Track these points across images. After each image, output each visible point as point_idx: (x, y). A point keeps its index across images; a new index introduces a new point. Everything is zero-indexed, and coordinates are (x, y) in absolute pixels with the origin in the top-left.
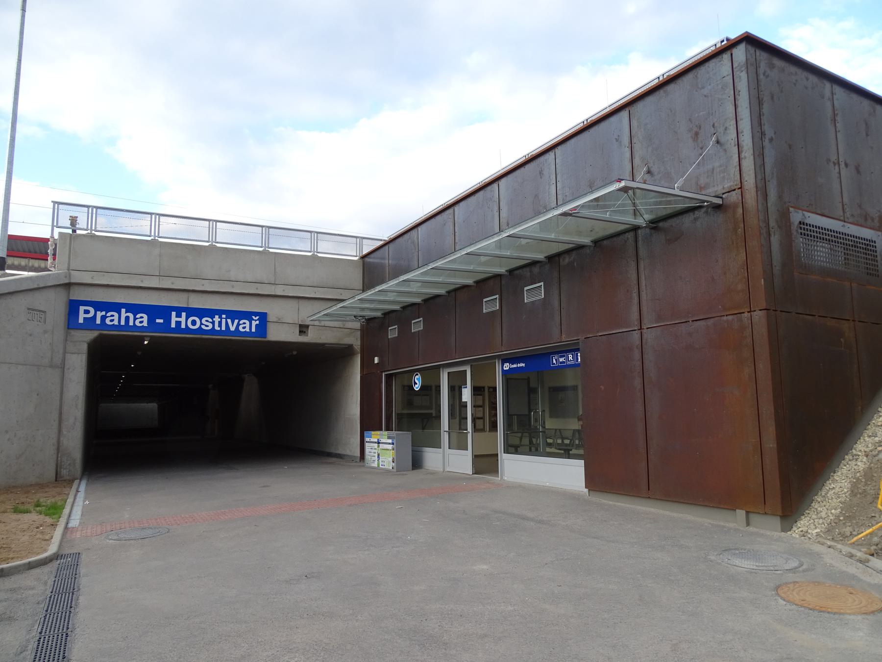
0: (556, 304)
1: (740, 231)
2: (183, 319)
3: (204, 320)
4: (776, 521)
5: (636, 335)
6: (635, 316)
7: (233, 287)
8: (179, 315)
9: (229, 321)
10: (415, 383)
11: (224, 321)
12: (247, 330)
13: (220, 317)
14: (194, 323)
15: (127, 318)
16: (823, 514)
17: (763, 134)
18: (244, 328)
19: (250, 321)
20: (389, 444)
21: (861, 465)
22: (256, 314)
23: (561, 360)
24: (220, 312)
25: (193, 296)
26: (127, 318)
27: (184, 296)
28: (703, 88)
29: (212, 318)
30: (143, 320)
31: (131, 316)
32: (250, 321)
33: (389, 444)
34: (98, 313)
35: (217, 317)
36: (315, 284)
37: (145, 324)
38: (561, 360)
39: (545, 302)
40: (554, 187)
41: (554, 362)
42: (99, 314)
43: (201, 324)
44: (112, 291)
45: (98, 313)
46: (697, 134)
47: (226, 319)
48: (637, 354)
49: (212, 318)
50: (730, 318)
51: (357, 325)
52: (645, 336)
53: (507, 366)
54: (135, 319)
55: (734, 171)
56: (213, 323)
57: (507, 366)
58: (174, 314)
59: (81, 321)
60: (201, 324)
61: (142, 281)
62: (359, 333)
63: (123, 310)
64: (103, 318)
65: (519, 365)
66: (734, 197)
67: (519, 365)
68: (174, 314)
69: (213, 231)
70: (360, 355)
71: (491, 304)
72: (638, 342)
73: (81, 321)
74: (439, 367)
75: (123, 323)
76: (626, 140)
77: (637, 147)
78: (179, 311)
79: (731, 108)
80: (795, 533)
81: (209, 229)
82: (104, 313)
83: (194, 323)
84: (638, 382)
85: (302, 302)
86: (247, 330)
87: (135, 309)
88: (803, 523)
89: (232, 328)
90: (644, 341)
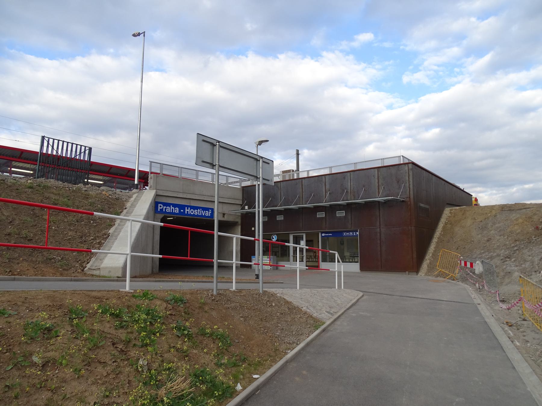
0: (350, 218)
1: (409, 208)
2: (189, 210)
3: (195, 210)
4: (415, 273)
5: (378, 230)
6: (378, 224)
7: (204, 198)
8: (188, 209)
9: (202, 211)
10: (273, 238)
11: (201, 211)
12: (208, 215)
13: (200, 210)
14: (192, 212)
15: (173, 209)
16: (423, 272)
17: (414, 185)
18: (168, 210)
19: (209, 211)
20: (264, 260)
21: (428, 261)
22: (210, 209)
23: (347, 234)
24: (200, 208)
25: (192, 201)
26: (173, 209)
27: (188, 201)
28: (400, 171)
29: (198, 210)
30: (177, 210)
31: (173, 208)
32: (209, 211)
33: (264, 260)
34: (164, 207)
35: (199, 209)
36: (228, 197)
37: (178, 212)
38: (347, 234)
39: (345, 217)
40: (349, 183)
41: (345, 234)
42: (164, 207)
43: (194, 212)
44: (168, 198)
45: (164, 207)
46: (398, 182)
47: (202, 210)
48: (379, 235)
49: (198, 210)
50: (406, 227)
51: (240, 214)
52: (381, 230)
53: (323, 235)
54: (175, 210)
55: (408, 193)
56: (198, 212)
57: (323, 235)
58: (186, 208)
59: (159, 210)
60: (194, 212)
61: (178, 195)
62: (240, 217)
63: (171, 206)
64: (166, 209)
65: (329, 235)
66: (408, 199)
67: (329, 235)
68: (186, 208)
69: (197, 175)
70: (240, 226)
71: (321, 215)
72: (379, 231)
73: (159, 210)
74: (289, 233)
75: (171, 211)
76: (376, 177)
77: (380, 180)
78: (188, 206)
79: (407, 178)
80: (418, 275)
81: (196, 176)
82: (165, 207)
83: (192, 212)
84: (379, 242)
85: (224, 205)
86: (208, 215)
87: (175, 206)
88: (420, 274)
89: (203, 215)
90: (381, 231)
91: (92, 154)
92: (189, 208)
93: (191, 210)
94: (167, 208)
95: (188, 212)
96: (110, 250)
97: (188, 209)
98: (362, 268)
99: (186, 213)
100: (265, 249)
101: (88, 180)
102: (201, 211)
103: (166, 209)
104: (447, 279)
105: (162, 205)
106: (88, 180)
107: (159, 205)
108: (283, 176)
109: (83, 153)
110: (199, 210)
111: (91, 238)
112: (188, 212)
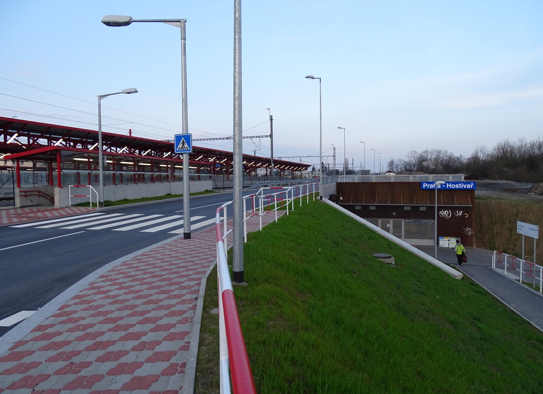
2: (450, 185)
8: (449, 184)
9: (464, 185)
13: (461, 184)
14: (453, 186)
32: (471, 184)
42: (428, 185)
49: (459, 184)
56: (459, 186)
64: (429, 186)
83: (453, 186)
91: (3, 139)
92: (450, 184)
93: (452, 185)
94: (431, 185)
95: (449, 187)
96: (214, 159)
97: (449, 184)
98: (244, 244)
99: (447, 187)
100: (506, 307)
101: (87, 140)
102: (462, 185)
103: (429, 186)
104: (67, 352)
105: (426, 184)
106: (87, 140)
107: (424, 184)
108: (220, 155)
109: (8, 140)
110: (460, 184)
111: (265, 375)
112: (449, 187)
